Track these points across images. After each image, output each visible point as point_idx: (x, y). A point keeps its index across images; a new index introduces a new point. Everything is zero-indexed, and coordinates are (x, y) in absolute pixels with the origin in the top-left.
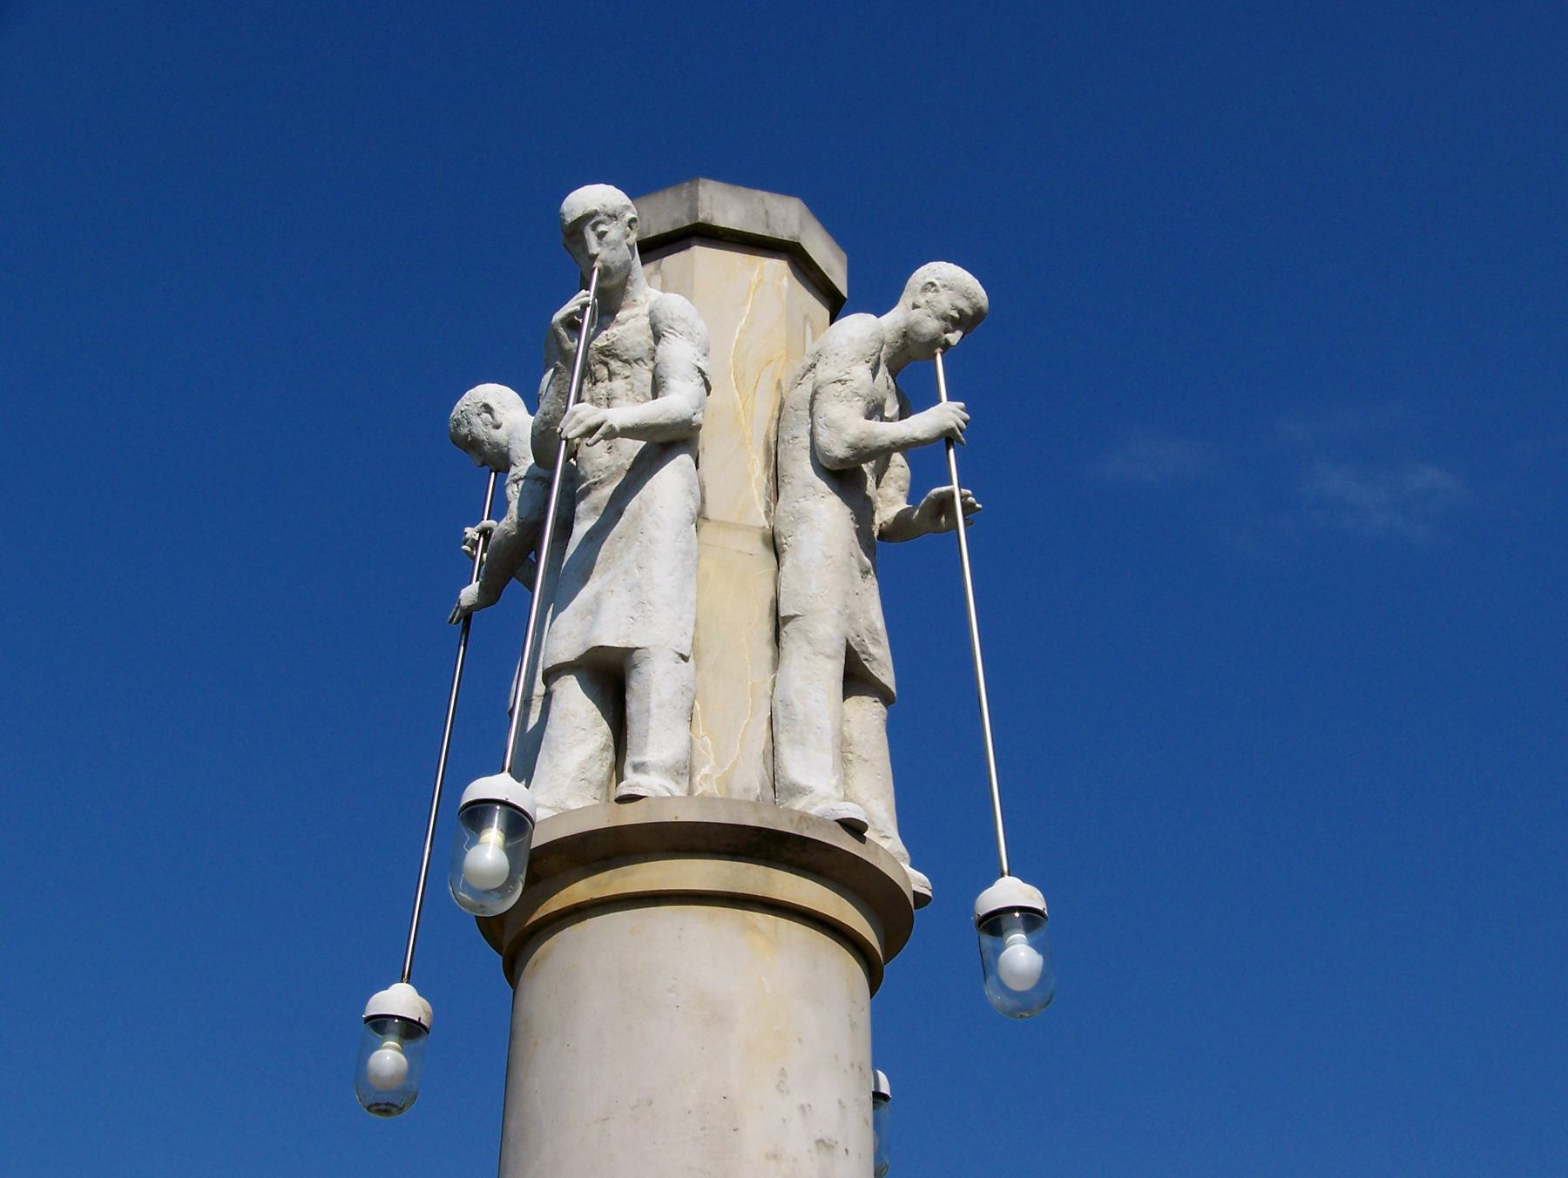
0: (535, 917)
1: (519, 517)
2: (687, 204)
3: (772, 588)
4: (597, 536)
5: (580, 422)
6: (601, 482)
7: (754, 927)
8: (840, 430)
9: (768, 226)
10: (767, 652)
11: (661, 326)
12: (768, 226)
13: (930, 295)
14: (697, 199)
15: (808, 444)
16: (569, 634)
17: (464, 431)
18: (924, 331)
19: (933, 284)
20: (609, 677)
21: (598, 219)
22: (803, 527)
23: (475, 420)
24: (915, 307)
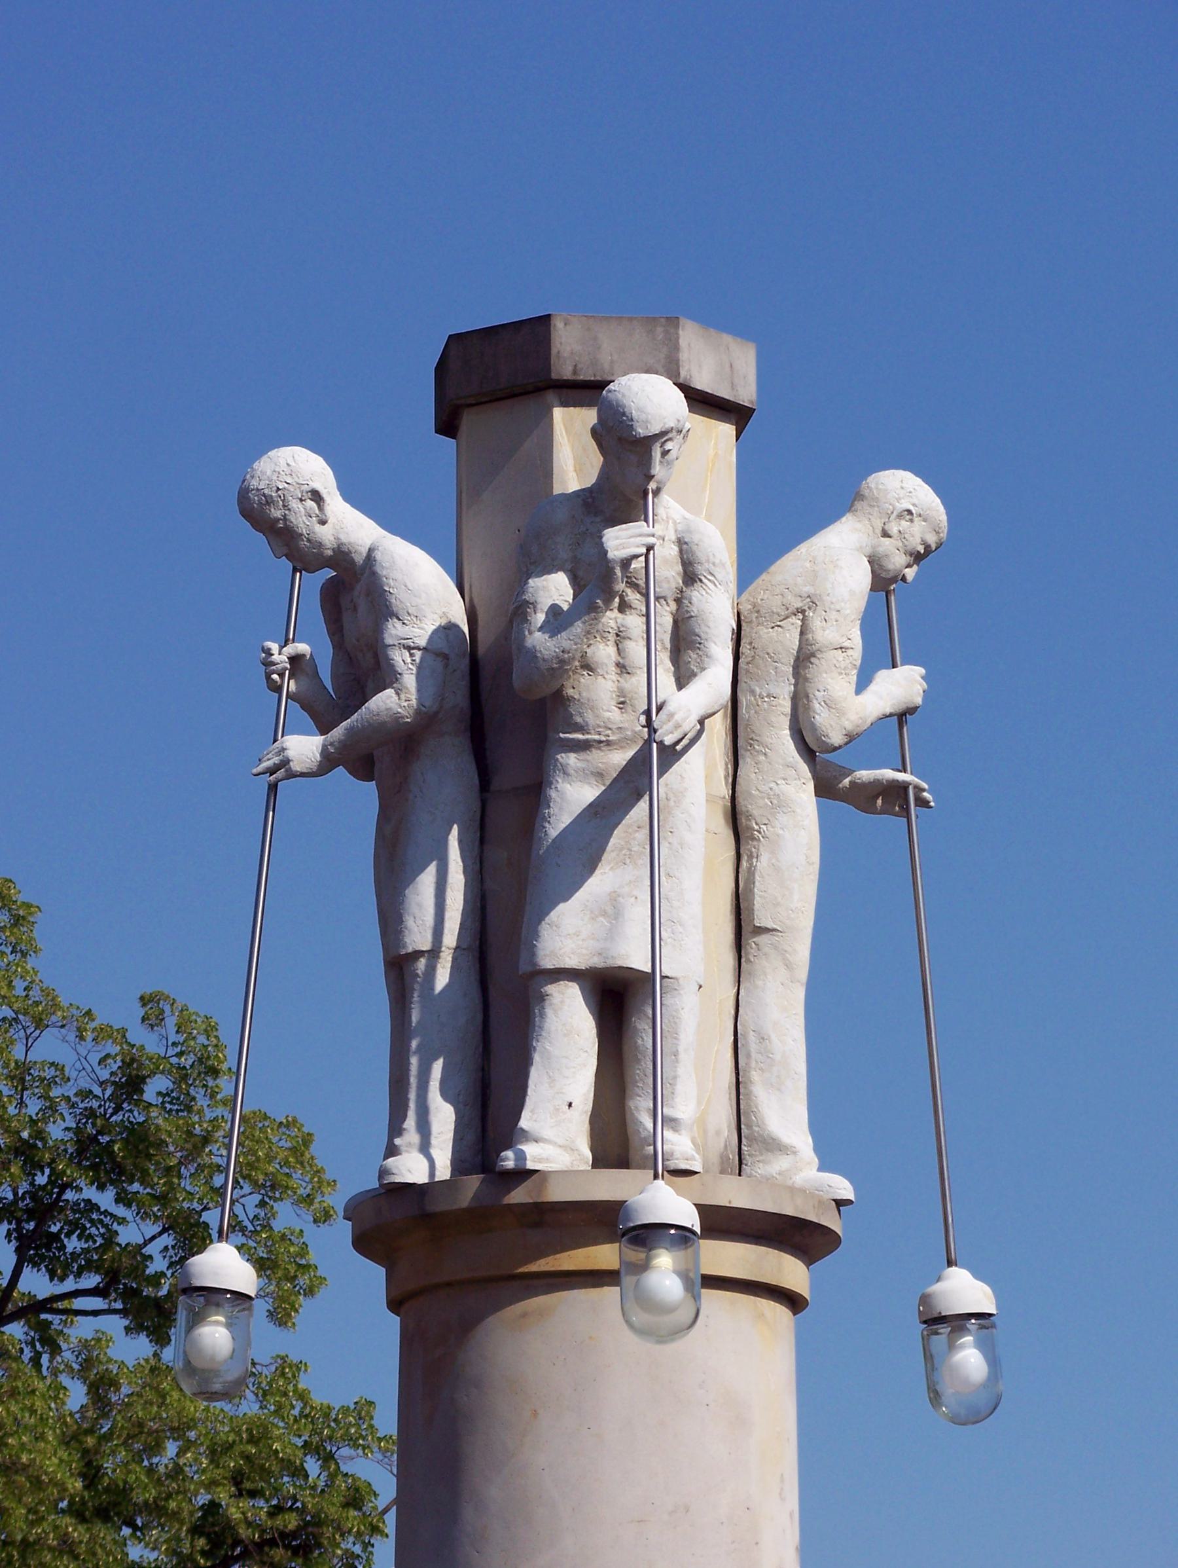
0: (520, 1270)
1: (419, 699)
2: (665, 350)
3: (733, 885)
4: (604, 815)
5: (678, 726)
6: (608, 743)
7: (761, 1316)
8: (841, 713)
9: (733, 386)
10: (728, 958)
11: (700, 569)
12: (733, 386)
13: (905, 524)
14: (676, 348)
15: (788, 710)
16: (577, 934)
17: (277, 513)
18: (891, 567)
19: (910, 512)
20: (618, 998)
21: (670, 435)
22: (783, 819)
23: (294, 504)
24: (886, 534)
